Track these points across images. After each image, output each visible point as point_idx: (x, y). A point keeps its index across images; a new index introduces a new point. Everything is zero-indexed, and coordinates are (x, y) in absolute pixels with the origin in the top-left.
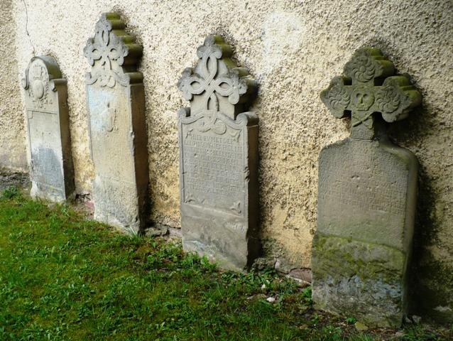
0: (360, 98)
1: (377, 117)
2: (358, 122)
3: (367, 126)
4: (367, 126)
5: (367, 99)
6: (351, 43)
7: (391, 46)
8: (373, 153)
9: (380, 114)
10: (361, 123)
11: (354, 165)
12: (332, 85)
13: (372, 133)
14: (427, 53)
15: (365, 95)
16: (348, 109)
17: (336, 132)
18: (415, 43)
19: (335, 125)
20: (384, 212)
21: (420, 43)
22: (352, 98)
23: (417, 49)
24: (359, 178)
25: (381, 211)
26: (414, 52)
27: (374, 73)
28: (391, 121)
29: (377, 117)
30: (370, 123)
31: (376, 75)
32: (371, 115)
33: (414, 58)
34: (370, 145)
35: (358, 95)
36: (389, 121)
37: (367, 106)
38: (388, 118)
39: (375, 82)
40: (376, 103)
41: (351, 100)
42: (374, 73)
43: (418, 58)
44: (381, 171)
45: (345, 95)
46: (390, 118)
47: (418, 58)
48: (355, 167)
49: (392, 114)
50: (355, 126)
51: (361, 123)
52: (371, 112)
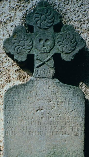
0: (42, 43)
1: (57, 57)
2: (42, 63)
3: (49, 66)
4: (49, 66)
5: (49, 43)
6: (22, 5)
7: (57, 7)
8: (55, 88)
9: (60, 55)
10: (44, 64)
11: (38, 100)
12: (15, 33)
13: (53, 72)
14: (85, 13)
15: (46, 40)
16: (31, 53)
17: (10, 81)
18: (76, 5)
19: (8, 76)
20: (66, 136)
21: (79, 4)
22: (34, 43)
23: (77, 9)
24: (43, 111)
25: (64, 135)
26: (75, 12)
27: (53, 21)
28: (70, 60)
29: (57, 57)
30: (52, 63)
31: (55, 23)
32: (52, 57)
33: (75, 16)
34: (51, 81)
35: (40, 40)
36: (68, 60)
37: (49, 49)
38: (65, 57)
39: (54, 29)
40: (57, 46)
41: (34, 45)
42: (53, 21)
43: (78, 16)
44: (62, 102)
45: (28, 41)
46: (68, 57)
47: (78, 16)
48: (39, 102)
49: (71, 54)
50: (38, 67)
51: (44, 64)
52: (52, 54)
